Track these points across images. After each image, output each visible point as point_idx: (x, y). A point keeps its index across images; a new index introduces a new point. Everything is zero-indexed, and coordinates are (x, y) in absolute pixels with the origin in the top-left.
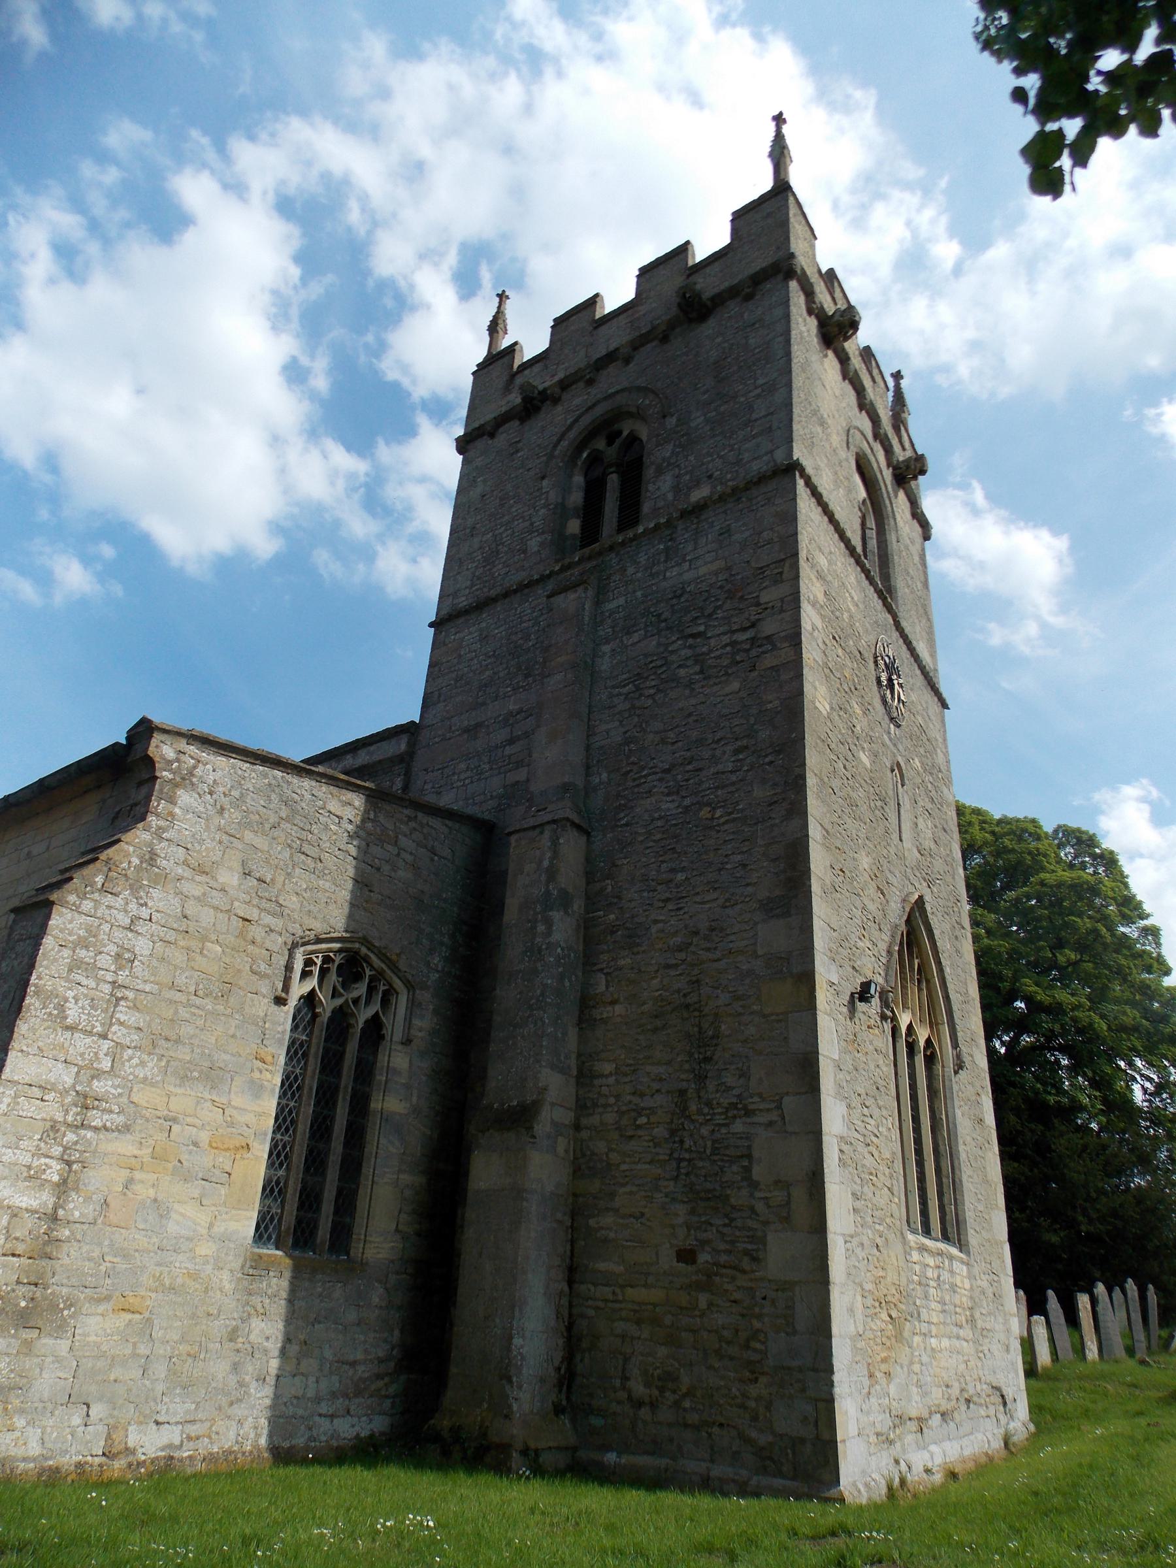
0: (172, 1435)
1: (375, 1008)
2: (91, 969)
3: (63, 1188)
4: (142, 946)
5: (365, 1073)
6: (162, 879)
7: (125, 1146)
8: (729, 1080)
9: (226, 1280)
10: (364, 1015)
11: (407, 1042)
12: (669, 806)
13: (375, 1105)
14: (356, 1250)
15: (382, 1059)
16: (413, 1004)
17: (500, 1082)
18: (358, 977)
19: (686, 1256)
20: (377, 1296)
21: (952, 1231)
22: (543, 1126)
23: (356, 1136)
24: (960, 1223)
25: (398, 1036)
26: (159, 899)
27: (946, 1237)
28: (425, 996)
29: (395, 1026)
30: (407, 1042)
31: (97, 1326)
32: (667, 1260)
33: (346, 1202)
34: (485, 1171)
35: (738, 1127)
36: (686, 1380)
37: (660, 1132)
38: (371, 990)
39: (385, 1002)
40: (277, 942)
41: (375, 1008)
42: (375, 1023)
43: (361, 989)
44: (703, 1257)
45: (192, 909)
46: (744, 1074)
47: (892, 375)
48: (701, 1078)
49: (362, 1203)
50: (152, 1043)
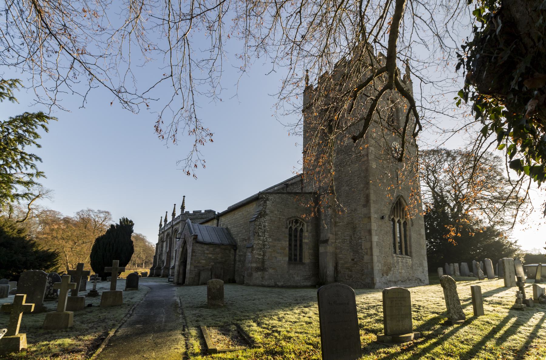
0: (282, 283)
1: (301, 227)
2: (261, 229)
3: (264, 255)
4: (267, 224)
5: (301, 236)
6: (267, 215)
7: (270, 250)
8: (358, 234)
9: (286, 266)
10: (299, 229)
11: (307, 231)
12: (347, 188)
13: (303, 241)
14: (303, 261)
15: (303, 234)
16: (308, 226)
17: (322, 237)
18: (298, 223)
19: (353, 260)
20: (307, 267)
21: (409, 254)
22: (329, 242)
23: (301, 246)
24: (411, 252)
25: (306, 230)
26: (267, 217)
27: (407, 254)
28: (309, 224)
29: (305, 228)
30: (307, 231)
31: (271, 271)
32: (350, 260)
33: (301, 255)
34: (322, 249)
35: (360, 241)
36: (353, 276)
37: (348, 242)
38: (300, 224)
39: (303, 226)
40: (284, 220)
41: (301, 227)
42: (302, 229)
43: (298, 224)
44: (355, 260)
45: (272, 218)
46: (360, 233)
47: (301, 261)
48: (354, 234)
49: (303, 255)
50: (270, 237)
